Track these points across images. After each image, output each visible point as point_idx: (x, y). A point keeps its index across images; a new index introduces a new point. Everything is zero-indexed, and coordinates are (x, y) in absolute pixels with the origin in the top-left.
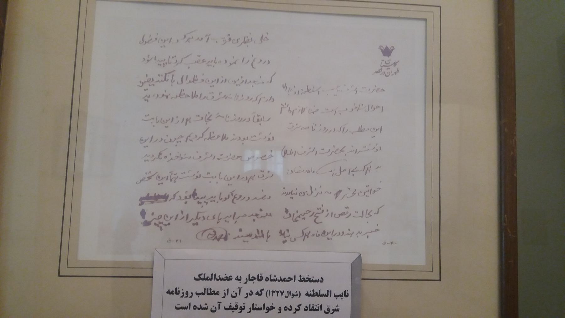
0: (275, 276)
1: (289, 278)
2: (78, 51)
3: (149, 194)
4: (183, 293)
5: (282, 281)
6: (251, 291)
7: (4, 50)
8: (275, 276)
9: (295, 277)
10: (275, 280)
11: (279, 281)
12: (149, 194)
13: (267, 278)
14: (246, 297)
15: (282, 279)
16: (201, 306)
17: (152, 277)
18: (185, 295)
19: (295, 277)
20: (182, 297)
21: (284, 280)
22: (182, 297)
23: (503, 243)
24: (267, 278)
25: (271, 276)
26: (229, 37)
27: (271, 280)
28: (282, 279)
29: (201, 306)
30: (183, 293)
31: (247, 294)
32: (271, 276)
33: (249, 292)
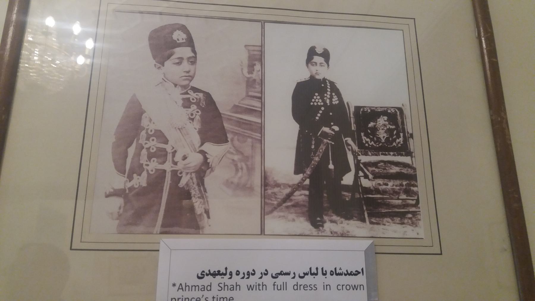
0: (340, 269)
1: (356, 271)
3: (106, 193)
4: (244, 274)
8: (340, 269)
9: (362, 269)
10: (341, 274)
11: (345, 275)
12: (106, 193)
13: (331, 271)
14: (261, 278)
15: (349, 272)
16: (209, 271)
18: (246, 276)
19: (362, 269)
20: (243, 278)
21: (351, 274)
22: (243, 278)
23: (488, 72)
24: (331, 271)
25: (335, 269)
26: (185, 63)
27: (337, 274)
28: (349, 272)
29: (209, 271)
30: (244, 274)
31: (262, 273)
32: (335, 269)
33: (264, 271)
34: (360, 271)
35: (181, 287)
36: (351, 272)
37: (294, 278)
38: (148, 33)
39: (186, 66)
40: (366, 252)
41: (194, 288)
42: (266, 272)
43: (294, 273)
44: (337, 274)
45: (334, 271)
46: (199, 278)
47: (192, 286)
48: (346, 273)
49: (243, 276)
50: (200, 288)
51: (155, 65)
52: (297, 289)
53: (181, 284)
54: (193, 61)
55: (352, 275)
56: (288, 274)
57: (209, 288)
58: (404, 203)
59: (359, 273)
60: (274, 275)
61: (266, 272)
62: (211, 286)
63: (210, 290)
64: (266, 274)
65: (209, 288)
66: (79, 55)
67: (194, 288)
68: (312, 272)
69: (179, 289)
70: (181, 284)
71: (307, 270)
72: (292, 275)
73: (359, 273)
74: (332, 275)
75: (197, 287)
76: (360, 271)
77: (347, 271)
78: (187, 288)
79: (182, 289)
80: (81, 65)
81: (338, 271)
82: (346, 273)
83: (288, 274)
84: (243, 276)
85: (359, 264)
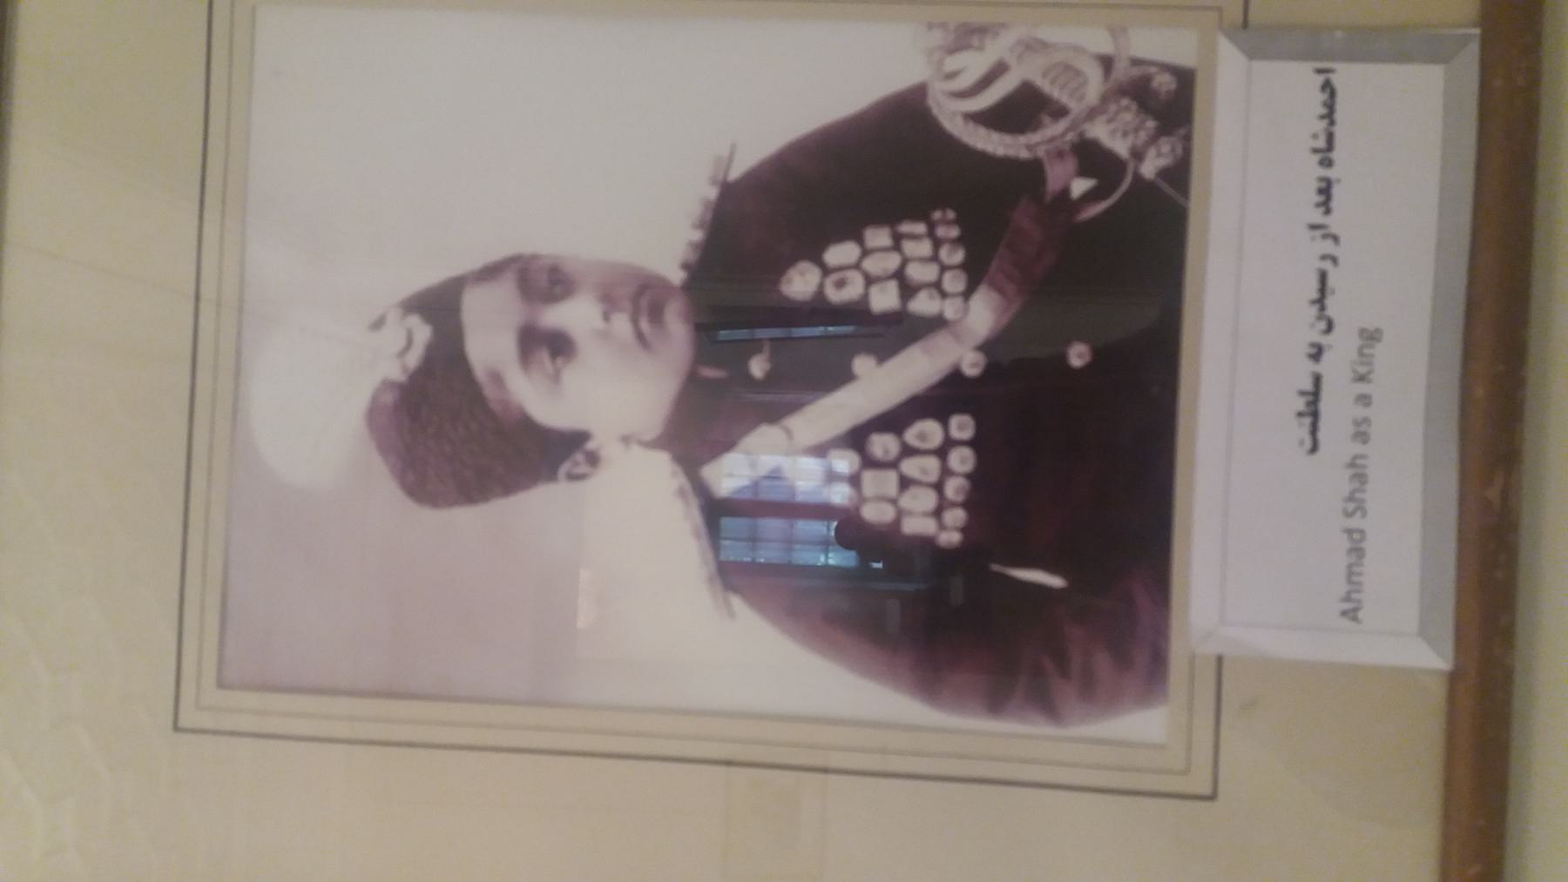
0: (1315, 136)
8: (1315, 136)
9: (1319, 71)
10: (1330, 138)
11: (1332, 123)
19: (1319, 71)
25: (1316, 151)
34: (1321, 79)
37: (1334, 260)
38: (410, 505)
39: (576, 315)
43: (1324, 257)
44: (1330, 145)
51: (573, 477)
54: (540, 280)
56: (1323, 277)
57: (1357, 536)
65: (1357, 536)
71: (1314, 310)
72: (1327, 265)
80: (787, 299)
81: (1321, 143)
83: (1323, 277)
85: (1295, 82)
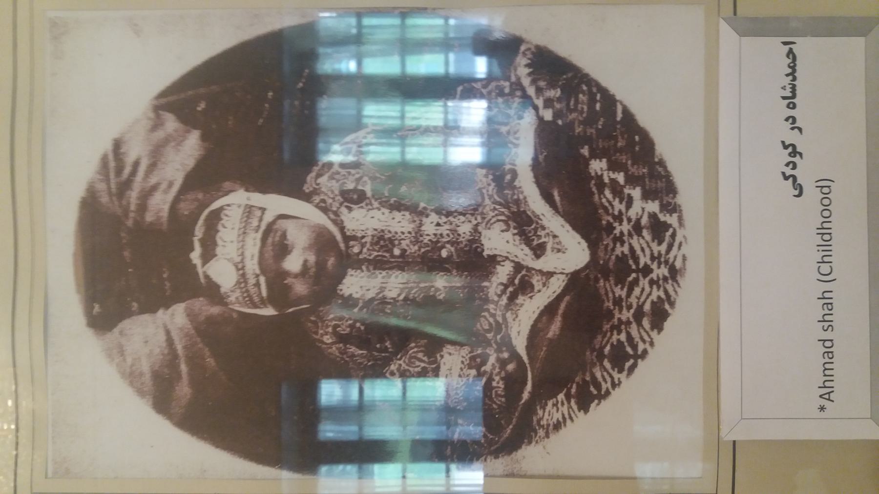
0: (784, 88)
1: (788, 56)
2: (9, 201)
5: (794, 71)
6: (787, 120)
7: (217, 447)
8: (784, 88)
9: (785, 43)
11: (794, 79)
13: (788, 107)
14: (800, 130)
15: (790, 71)
17: (734, 442)
19: (785, 43)
21: (793, 67)
24: (788, 107)
25: (784, 98)
27: (794, 96)
28: (790, 71)
31: (792, 129)
32: (784, 98)
33: (788, 125)
35: (827, 396)
36: (789, 67)
40: (742, 33)
41: (827, 372)
42: (791, 120)
45: (788, 101)
46: (800, 195)
47: (825, 375)
48: (791, 78)
49: (796, 130)
50: (828, 360)
52: (830, 234)
53: (821, 396)
55: (795, 65)
57: (828, 344)
58: (523, 48)
59: (791, 51)
60: (797, 192)
61: (791, 120)
62: (825, 341)
63: (831, 340)
64: (794, 120)
66: (195, 128)
67: (827, 372)
68: (790, 95)
69: (829, 399)
70: (821, 396)
73: (791, 51)
74: (794, 107)
75: (827, 366)
76: (787, 47)
77: (787, 75)
78: (827, 384)
79: (829, 393)
82: (791, 78)
84: (796, 130)
85: (774, 47)
